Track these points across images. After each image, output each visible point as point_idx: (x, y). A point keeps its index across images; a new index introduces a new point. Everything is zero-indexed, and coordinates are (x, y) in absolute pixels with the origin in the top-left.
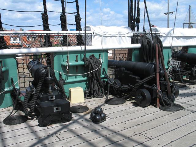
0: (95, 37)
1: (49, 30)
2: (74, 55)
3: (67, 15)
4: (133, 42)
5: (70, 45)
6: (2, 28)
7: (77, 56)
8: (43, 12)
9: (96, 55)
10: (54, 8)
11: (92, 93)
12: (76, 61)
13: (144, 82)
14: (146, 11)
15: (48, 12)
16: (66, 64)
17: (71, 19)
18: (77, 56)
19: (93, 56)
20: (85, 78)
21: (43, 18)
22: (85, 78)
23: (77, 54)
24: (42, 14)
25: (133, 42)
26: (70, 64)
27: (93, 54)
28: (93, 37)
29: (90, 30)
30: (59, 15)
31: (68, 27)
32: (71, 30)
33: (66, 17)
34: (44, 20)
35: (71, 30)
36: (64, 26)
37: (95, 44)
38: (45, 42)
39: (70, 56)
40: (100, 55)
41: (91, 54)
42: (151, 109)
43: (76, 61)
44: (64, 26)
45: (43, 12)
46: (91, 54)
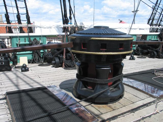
0: (37, 28)
1: (22, 24)
2: (24, 39)
3: (21, 15)
4: (150, 32)
5: (24, 33)
6: (21, 23)
7: (25, 39)
8: (6, 13)
9: (38, 39)
10: (12, 11)
11: (35, 60)
12: (25, 42)
13: (58, 54)
14: (74, 14)
15: (20, 14)
16: (18, 43)
17: (23, 18)
18: (25, 39)
19: (35, 39)
20: (32, 52)
21: (6, 17)
22: (32, 52)
23: (25, 38)
24: (26, 16)
25: (150, 32)
26: (21, 43)
27: (35, 38)
28: (35, 28)
29: (34, 24)
30: (16, 15)
31: (22, 22)
32: (24, 23)
33: (20, 16)
34: (7, 18)
35: (24, 23)
36: (19, 22)
37: (37, 32)
38: (9, 31)
39: (21, 39)
40: (40, 39)
41: (34, 38)
42: (60, 69)
43: (25, 42)
44: (19, 22)
45: (6, 13)
46: (34, 38)
